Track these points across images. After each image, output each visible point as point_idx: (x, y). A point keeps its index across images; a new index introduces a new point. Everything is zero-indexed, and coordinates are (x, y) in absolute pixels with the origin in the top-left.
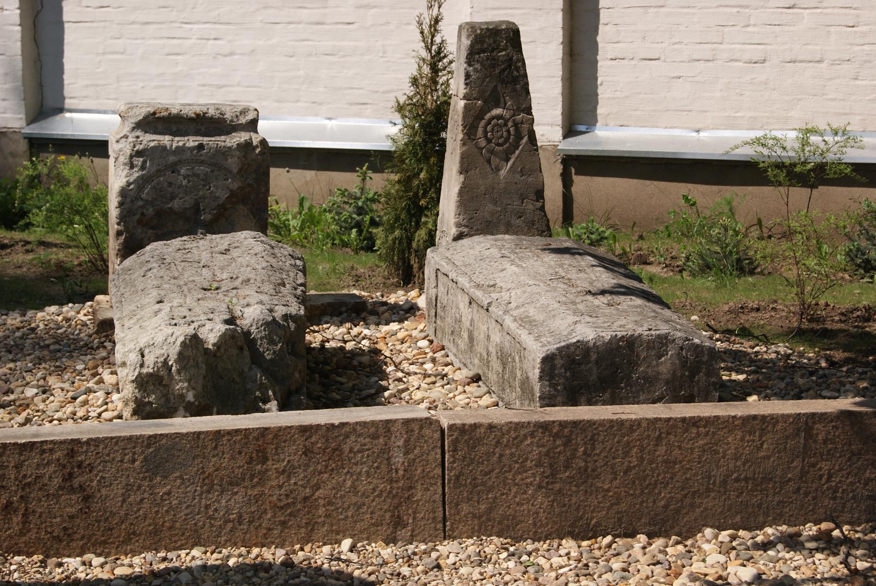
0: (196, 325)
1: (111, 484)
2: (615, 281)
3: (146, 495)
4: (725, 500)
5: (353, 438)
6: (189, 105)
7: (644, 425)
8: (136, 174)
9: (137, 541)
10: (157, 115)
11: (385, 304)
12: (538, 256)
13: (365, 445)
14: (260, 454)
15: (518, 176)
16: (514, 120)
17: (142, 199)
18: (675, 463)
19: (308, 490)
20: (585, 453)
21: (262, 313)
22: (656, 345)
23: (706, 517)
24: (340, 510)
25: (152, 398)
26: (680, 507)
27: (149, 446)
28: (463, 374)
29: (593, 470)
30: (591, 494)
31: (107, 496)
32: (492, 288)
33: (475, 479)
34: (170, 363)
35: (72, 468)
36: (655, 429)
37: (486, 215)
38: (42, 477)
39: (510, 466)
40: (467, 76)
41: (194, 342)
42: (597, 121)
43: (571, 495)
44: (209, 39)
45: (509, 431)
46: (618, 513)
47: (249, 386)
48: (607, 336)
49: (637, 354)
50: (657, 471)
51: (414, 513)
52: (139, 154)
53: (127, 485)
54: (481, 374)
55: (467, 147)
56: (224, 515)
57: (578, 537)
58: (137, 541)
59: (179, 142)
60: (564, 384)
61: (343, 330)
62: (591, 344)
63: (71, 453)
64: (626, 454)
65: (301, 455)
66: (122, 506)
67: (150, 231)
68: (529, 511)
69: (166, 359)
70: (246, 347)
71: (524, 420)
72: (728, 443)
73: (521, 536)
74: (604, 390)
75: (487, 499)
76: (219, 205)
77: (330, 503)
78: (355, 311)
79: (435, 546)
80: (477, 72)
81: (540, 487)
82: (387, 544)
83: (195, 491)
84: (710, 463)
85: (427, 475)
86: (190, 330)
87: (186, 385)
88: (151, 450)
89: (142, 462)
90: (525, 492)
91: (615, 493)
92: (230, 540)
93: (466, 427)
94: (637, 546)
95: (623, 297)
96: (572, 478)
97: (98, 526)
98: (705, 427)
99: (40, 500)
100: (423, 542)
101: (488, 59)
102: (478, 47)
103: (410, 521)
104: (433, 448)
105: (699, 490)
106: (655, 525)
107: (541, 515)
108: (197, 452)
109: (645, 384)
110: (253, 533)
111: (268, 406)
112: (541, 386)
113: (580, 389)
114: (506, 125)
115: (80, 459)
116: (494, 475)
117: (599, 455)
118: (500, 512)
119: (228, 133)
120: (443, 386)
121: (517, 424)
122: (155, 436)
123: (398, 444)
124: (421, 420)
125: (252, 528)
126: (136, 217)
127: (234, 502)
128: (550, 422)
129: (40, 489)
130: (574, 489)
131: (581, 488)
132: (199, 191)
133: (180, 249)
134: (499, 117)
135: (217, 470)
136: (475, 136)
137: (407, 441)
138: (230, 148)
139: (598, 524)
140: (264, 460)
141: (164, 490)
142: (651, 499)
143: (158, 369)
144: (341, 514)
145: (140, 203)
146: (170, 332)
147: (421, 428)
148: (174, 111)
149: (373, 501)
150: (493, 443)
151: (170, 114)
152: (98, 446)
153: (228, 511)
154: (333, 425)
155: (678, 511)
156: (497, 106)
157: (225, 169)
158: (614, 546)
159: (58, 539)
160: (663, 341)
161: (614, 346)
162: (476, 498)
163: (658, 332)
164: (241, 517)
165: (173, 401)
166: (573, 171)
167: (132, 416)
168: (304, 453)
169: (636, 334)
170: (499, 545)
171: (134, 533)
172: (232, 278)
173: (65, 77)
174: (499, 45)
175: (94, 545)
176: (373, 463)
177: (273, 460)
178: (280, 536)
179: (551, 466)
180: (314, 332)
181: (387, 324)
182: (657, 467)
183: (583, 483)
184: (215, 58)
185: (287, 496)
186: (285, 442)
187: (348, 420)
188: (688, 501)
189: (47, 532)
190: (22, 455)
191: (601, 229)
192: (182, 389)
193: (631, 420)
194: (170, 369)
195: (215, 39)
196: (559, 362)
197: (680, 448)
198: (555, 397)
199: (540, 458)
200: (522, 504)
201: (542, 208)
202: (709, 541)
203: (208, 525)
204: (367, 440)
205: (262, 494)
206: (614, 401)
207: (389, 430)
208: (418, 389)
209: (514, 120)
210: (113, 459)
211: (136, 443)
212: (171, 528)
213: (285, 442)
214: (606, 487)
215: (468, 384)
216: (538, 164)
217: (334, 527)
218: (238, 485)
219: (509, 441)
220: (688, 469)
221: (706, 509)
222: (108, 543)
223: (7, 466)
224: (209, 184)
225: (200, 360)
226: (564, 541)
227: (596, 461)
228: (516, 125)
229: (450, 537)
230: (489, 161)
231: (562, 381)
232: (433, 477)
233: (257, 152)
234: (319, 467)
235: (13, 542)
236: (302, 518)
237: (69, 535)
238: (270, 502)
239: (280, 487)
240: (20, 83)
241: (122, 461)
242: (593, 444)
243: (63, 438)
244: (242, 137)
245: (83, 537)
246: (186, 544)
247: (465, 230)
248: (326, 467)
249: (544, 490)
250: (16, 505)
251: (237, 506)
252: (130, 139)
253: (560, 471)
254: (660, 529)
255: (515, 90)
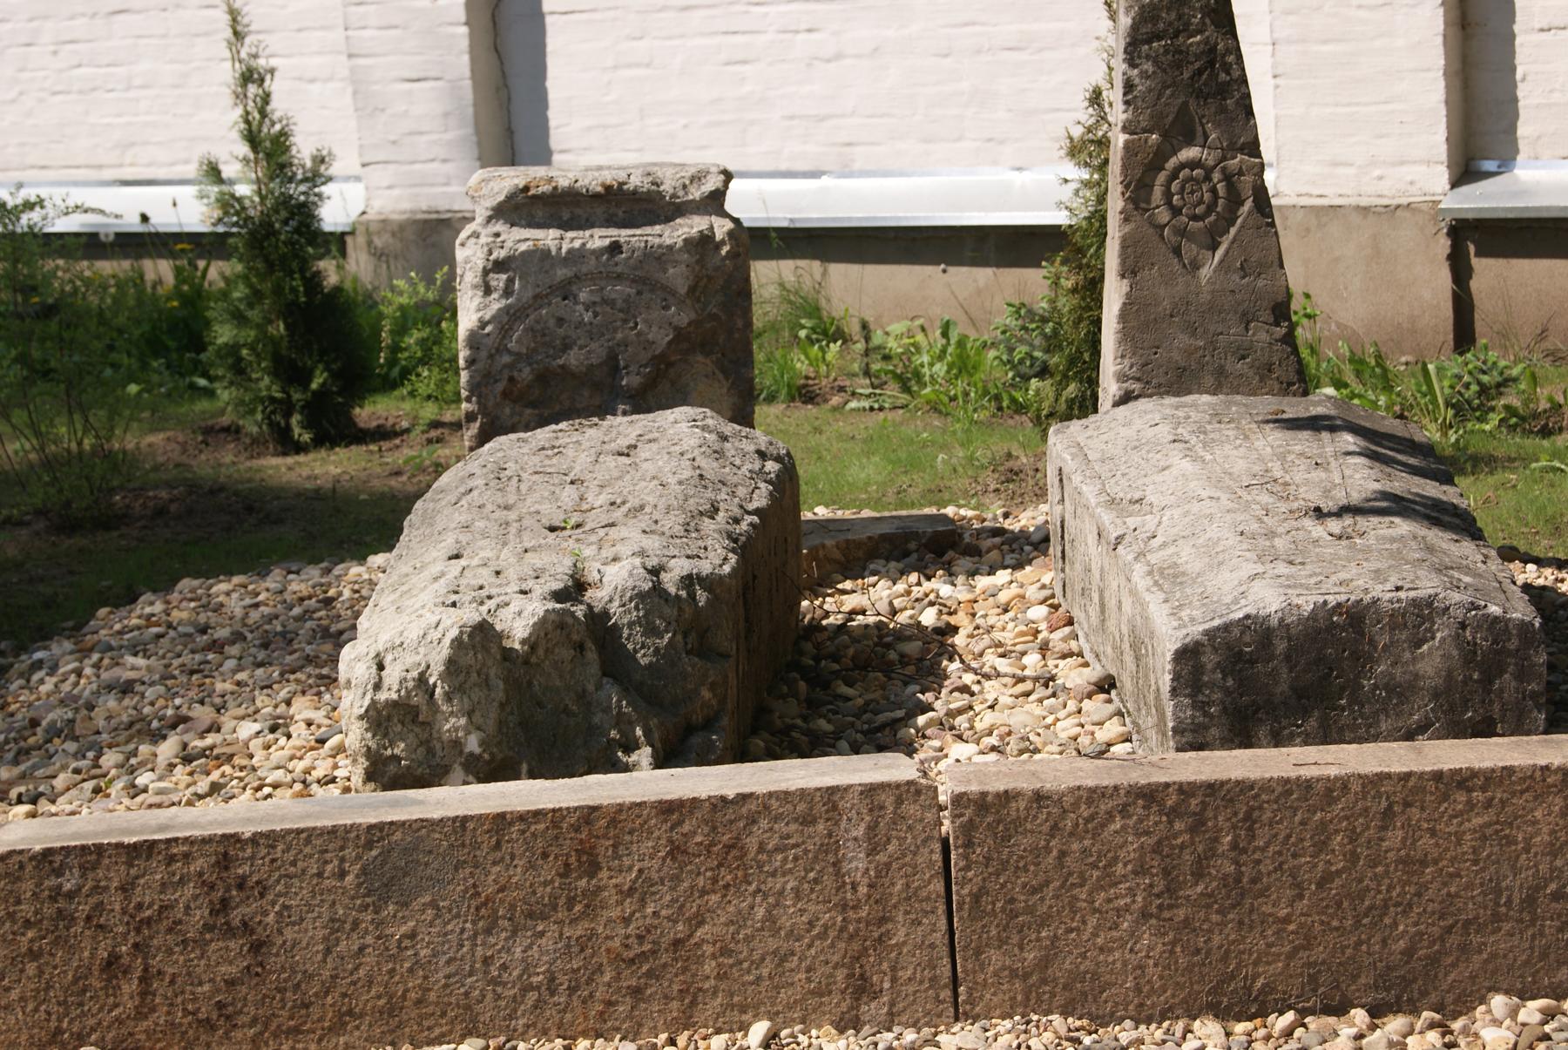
0: (491, 604)
1: (302, 920)
2: (1377, 486)
3: (369, 940)
4: (1533, 937)
5: (764, 823)
6: (600, 168)
7: (1355, 787)
8: (496, 304)
9: (357, 1028)
10: (532, 192)
11: (999, 532)
12: (1246, 437)
13: (788, 837)
14: (584, 858)
15: (1236, 277)
16: (1224, 170)
17: (509, 351)
18: (1424, 863)
19: (680, 927)
20: (1234, 846)
21: (631, 575)
22: (1410, 620)
23: (1494, 973)
24: (745, 965)
25: (400, 749)
26: (1438, 952)
27: (369, 845)
28: (1073, 676)
29: (1254, 881)
30: (1251, 928)
31: (295, 944)
32: (1137, 506)
33: (1012, 900)
34: (431, 681)
35: (228, 890)
36: (1379, 795)
37: (1176, 356)
38: (173, 907)
39: (1081, 875)
40: (1129, 86)
41: (482, 635)
42: (1517, 151)
43: (1210, 931)
44: (797, 32)
45: (1076, 805)
46: (1309, 965)
47: (596, 720)
48: (1307, 603)
49: (1371, 640)
50: (1387, 881)
51: (894, 969)
52: (499, 266)
53: (332, 920)
54: (1113, 672)
55: (1132, 225)
56: (521, 976)
57: (1224, 1014)
58: (357, 1028)
59: (573, 240)
60: (1223, 702)
61: (901, 587)
62: (1274, 622)
63: (224, 863)
64: (1321, 846)
65: (664, 859)
66: (324, 961)
67: (528, 411)
68: (1125, 963)
69: (422, 674)
70: (589, 645)
71: (1105, 783)
72: (1535, 823)
73: (1112, 1014)
74: (1306, 713)
75: (1038, 940)
76: (654, 358)
77: (725, 951)
78: (939, 548)
79: (936, 1034)
80: (1148, 77)
81: (1145, 915)
82: (841, 1031)
83: (463, 930)
84: (1498, 862)
85: (915, 893)
86: (470, 615)
87: (463, 721)
88: (374, 853)
89: (357, 876)
90: (1116, 926)
91: (1301, 926)
92: (534, 1025)
93: (989, 798)
94: (1346, 1032)
95: (1375, 520)
96: (1210, 896)
97: (282, 1000)
98: (1484, 789)
99: (170, 952)
100: (914, 1025)
101: (1166, 52)
102: (1146, 29)
103: (886, 985)
104: (925, 841)
105: (1476, 918)
106: (1388, 990)
107: (1150, 970)
108: (462, 855)
109: (1389, 697)
110: (579, 1011)
111: (634, 757)
112: (1175, 706)
113: (1256, 712)
114: (1208, 178)
115: (240, 871)
116: (1049, 892)
117: (1263, 849)
118: (1067, 966)
119: (668, 220)
120: (1040, 701)
121: (1092, 790)
122: (380, 827)
123: (855, 834)
124: (898, 786)
125: (576, 1002)
126: (500, 387)
127: (541, 950)
128: (1158, 785)
129: (170, 930)
130: (1215, 918)
131: (1231, 916)
132: (615, 330)
133: (543, 449)
134: (1193, 164)
135: (502, 890)
136: (1149, 202)
137: (872, 828)
138: (670, 248)
139: (1268, 989)
140: (593, 868)
141: (403, 929)
142: (1378, 938)
143: (408, 692)
144: (749, 972)
145: (506, 359)
146: (435, 619)
147: (899, 801)
148: (564, 183)
149: (810, 946)
150: (1046, 828)
151: (555, 188)
152: (274, 847)
153: (527, 970)
154: (723, 799)
155: (1434, 960)
156: (1189, 142)
157: (664, 288)
158: (1299, 1032)
159: (208, 1024)
160: (1423, 612)
161: (1322, 624)
162: (1015, 939)
163: (1412, 594)
164: (552, 979)
165: (440, 753)
166: (1472, 249)
167: (364, 783)
168: (670, 853)
169: (1367, 599)
170: (1063, 1031)
171: (350, 1012)
172: (612, 504)
173: (551, 114)
174: (1188, 24)
175: (275, 1036)
176: (807, 871)
177: (609, 869)
178: (630, 1017)
179: (1166, 872)
180: (844, 592)
181: (991, 572)
182: (1387, 872)
183: (1233, 906)
184: (809, 65)
185: (640, 938)
186: (631, 833)
187: (753, 790)
188: (1454, 940)
189: (186, 1012)
190: (132, 866)
191: (1502, 363)
192: (457, 730)
193: (1328, 779)
194: (431, 693)
195: (809, 31)
196: (1209, 659)
197: (1433, 832)
198: (1206, 728)
199: (1142, 857)
200: (1111, 950)
201: (1289, 339)
202: (1497, 1023)
203: (490, 996)
204: (793, 827)
205: (593, 934)
206: (1327, 736)
207: (835, 807)
208: (992, 707)
209: (1224, 170)
210: (304, 871)
211: (345, 839)
212: (419, 1002)
213: (631, 833)
214: (1283, 913)
215: (1089, 696)
216: (1275, 252)
217: (736, 999)
218: (544, 917)
219: (1077, 825)
220: (1451, 875)
221: (1494, 956)
222: (302, 1032)
223: (106, 888)
224: (635, 317)
225: (492, 672)
226: (1197, 1023)
227: (1258, 862)
228: (1227, 177)
229: (967, 1016)
230: (1177, 251)
231: (1217, 696)
232: (928, 899)
233: (723, 252)
234: (701, 881)
235: (124, 1031)
236: (671, 981)
237: (228, 1018)
238: (608, 951)
239: (626, 921)
240: (470, 130)
241: (320, 875)
242: (1250, 829)
243: (206, 833)
244: (695, 225)
245: (254, 1021)
246: (451, 1032)
247: (1136, 386)
248: (715, 880)
249: (1153, 921)
250: (125, 960)
251: (545, 958)
252: (483, 240)
253: (1185, 882)
254: (1399, 998)
255: (1223, 110)
